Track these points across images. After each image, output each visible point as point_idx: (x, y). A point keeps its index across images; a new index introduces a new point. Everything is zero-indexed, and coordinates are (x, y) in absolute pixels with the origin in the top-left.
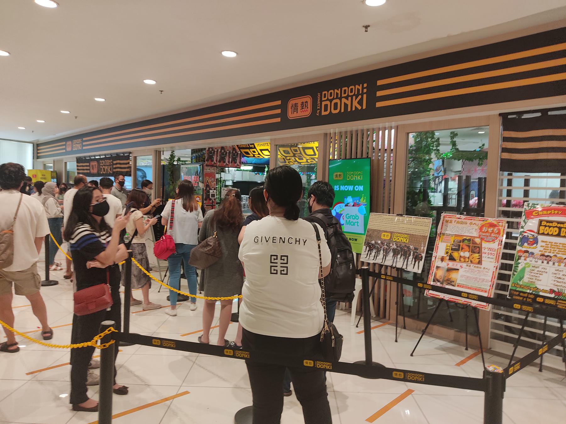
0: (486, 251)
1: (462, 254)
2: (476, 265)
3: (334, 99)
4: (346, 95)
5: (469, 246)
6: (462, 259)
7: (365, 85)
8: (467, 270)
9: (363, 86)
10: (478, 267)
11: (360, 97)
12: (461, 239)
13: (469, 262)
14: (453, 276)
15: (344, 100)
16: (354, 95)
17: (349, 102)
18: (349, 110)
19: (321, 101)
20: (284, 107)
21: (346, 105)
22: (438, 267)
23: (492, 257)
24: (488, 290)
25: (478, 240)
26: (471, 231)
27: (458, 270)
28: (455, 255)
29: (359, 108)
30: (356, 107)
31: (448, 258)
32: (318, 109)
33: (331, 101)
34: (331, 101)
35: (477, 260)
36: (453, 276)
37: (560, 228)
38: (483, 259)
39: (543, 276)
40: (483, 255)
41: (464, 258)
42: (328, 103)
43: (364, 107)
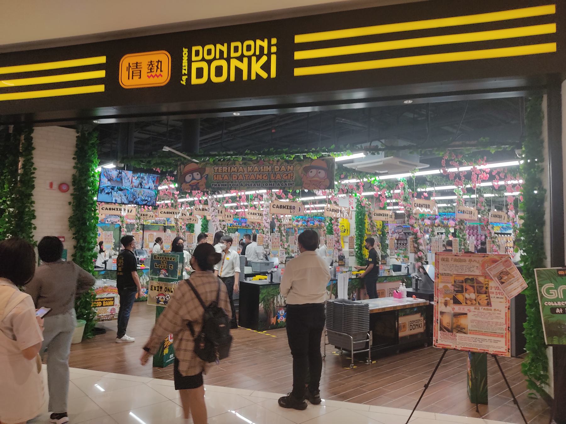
0: (493, 290)
1: (467, 296)
2: (486, 308)
3: (215, 59)
4: (238, 54)
5: (473, 287)
6: (468, 302)
7: (274, 41)
8: (476, 313)
9: (269, 42)
10: (488, 310)
11: (264, 59)
12: (462, 279)
13: (477, 305)
14: (463, 321)
15: (234, 63)
16: (254, 54)
17: (244, 66)
18: (245, 77)
19: (190, 61)
20: (112, 68)
21: (239, 72)
22: (442, 313)
23: (500, 296)
24: (504, 334)
25: (481, 279)
26: (472, 269)
27: (466, 314)
28: (460, 297)
29: (264, 75)
30: (257, 75)
31: (452, 301)
32: (185, 75)
33: (209, 62)
34: (209, 62)
35: (486, 302)
36: (463, 321)
37: (102, 302)
38: (492, 300)
39: (1, 128)
40: (491, 295)
41: (471, 300)
42: (204, 65)
43: (273, 74)
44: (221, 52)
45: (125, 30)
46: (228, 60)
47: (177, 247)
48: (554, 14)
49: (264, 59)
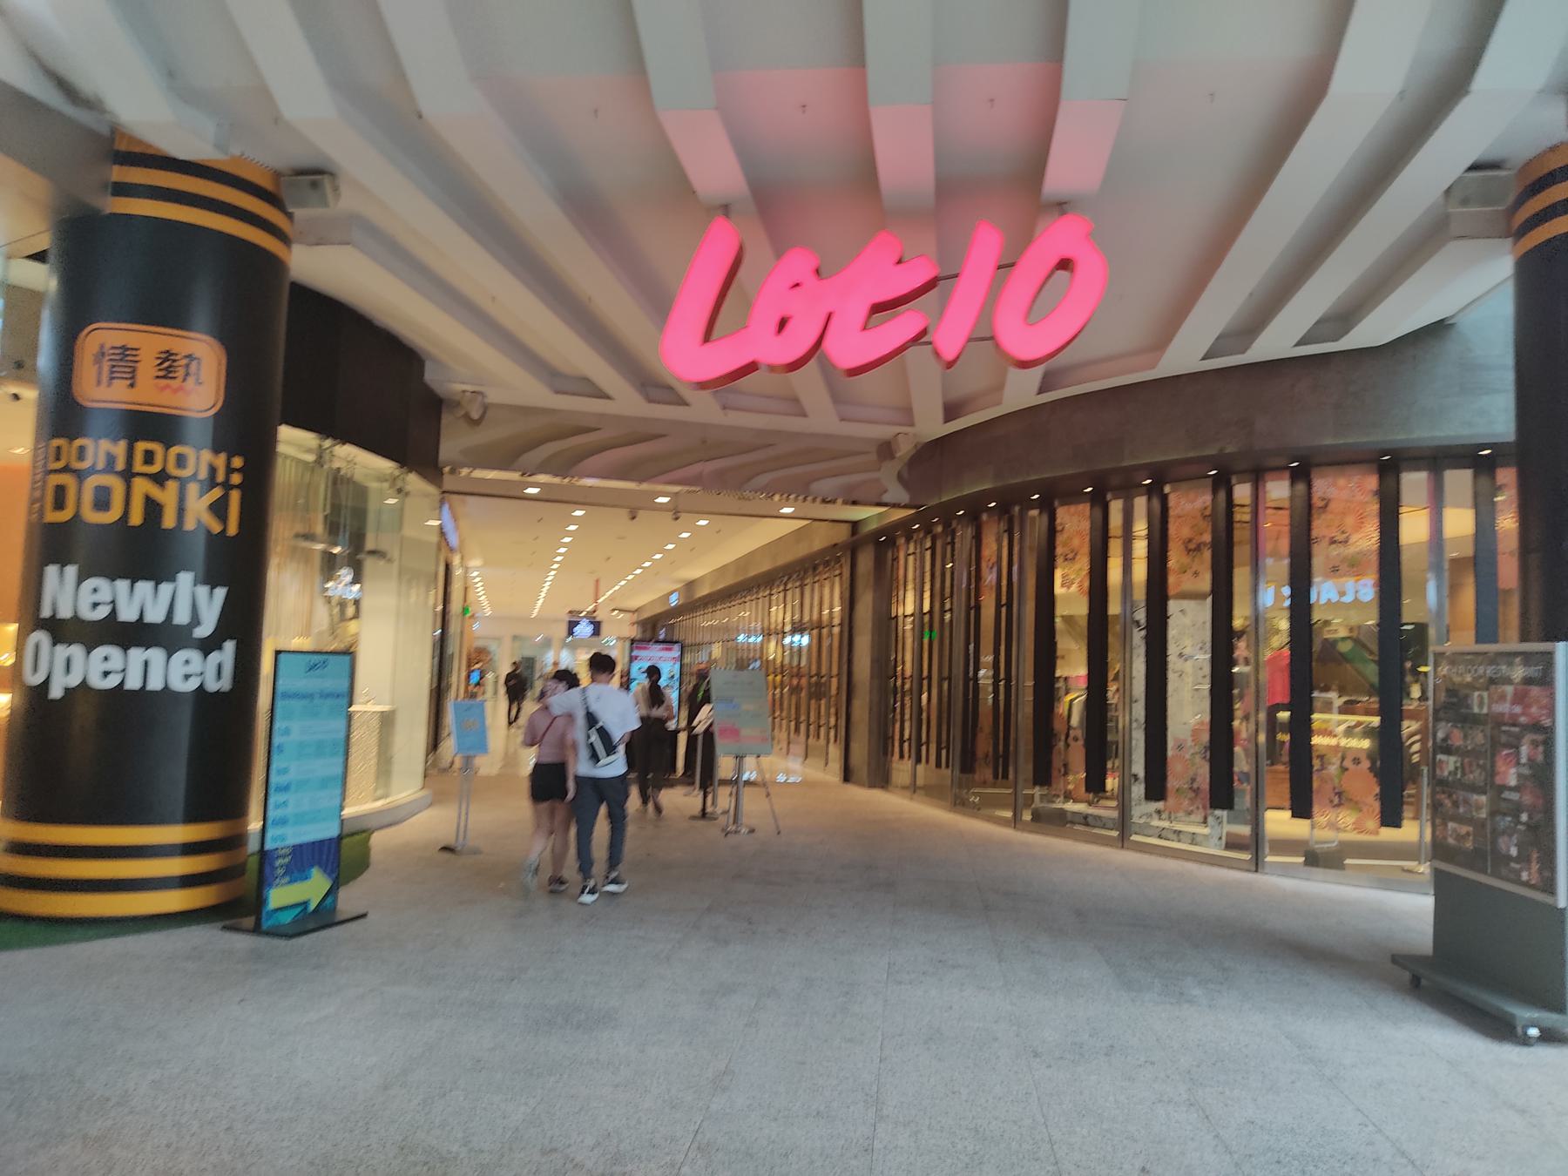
15: (141, 487)
21: (153, 509)
33: (80, 475)
43: (233, 530)
44: (111, 460)
45: (1334, 249)
46: (128, 475)
47: (655, 695)
48: (1426, 958)
49: (217, 493)
